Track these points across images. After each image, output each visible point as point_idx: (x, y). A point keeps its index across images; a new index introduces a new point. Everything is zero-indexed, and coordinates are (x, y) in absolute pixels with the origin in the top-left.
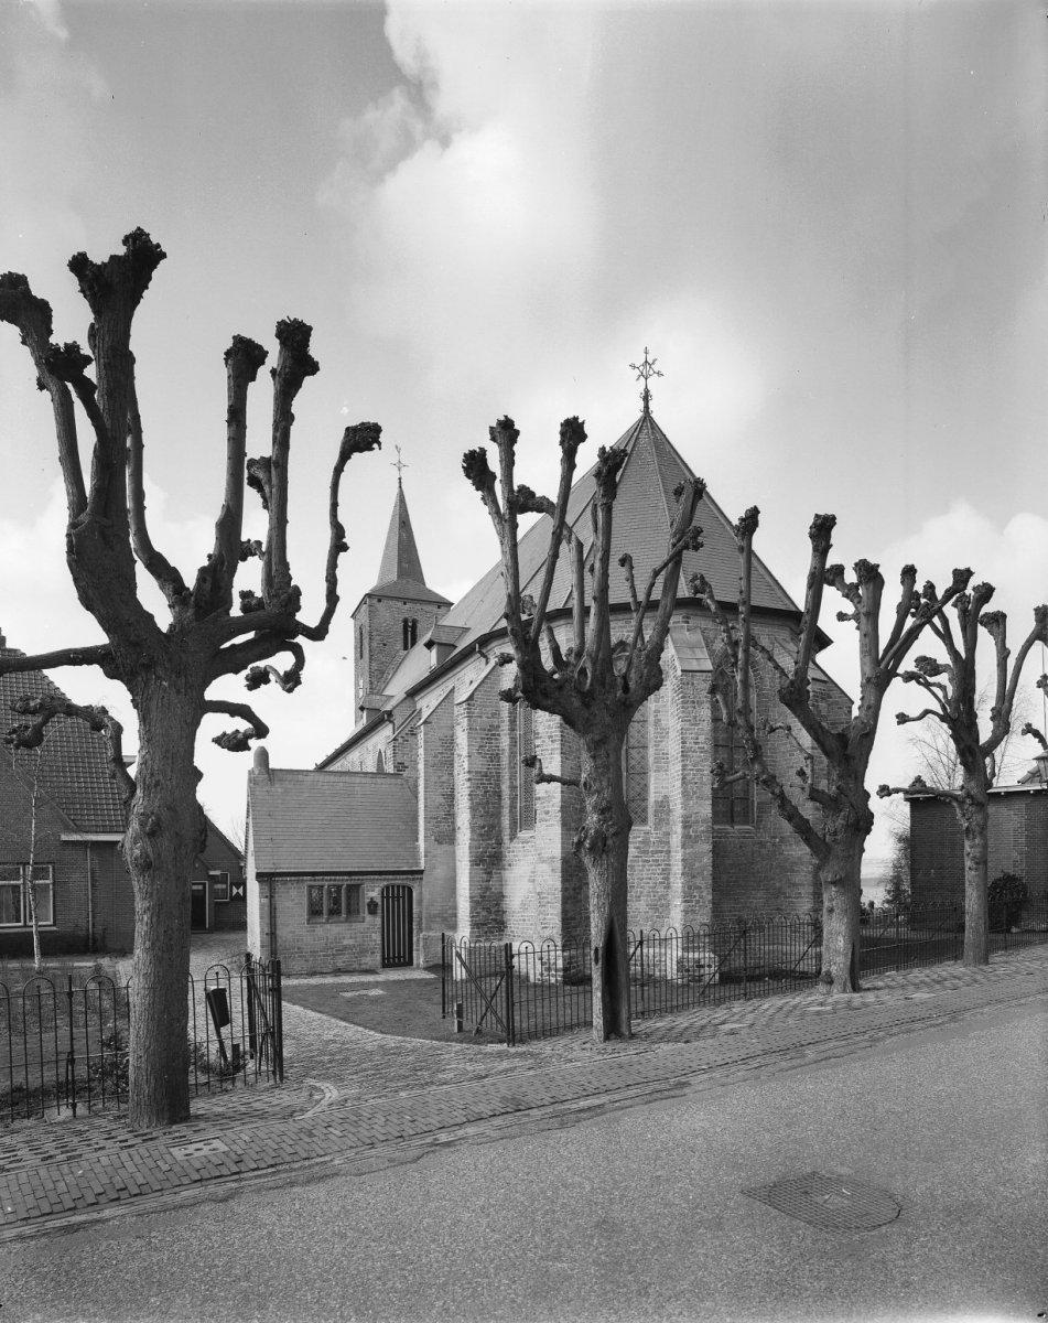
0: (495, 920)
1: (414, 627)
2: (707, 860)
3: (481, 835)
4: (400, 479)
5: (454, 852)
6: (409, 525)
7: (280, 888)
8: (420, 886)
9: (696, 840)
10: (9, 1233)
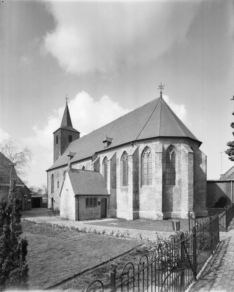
0: (137, 206)
1: (71, 137)
2: (193, 192)
3: (135, 186)
4: (67, 102)
5: (116, 190)
6: (69, 113)
7: (80, 199)
8: (109, 198)
9: (191, 188)
10: (176, 291)
